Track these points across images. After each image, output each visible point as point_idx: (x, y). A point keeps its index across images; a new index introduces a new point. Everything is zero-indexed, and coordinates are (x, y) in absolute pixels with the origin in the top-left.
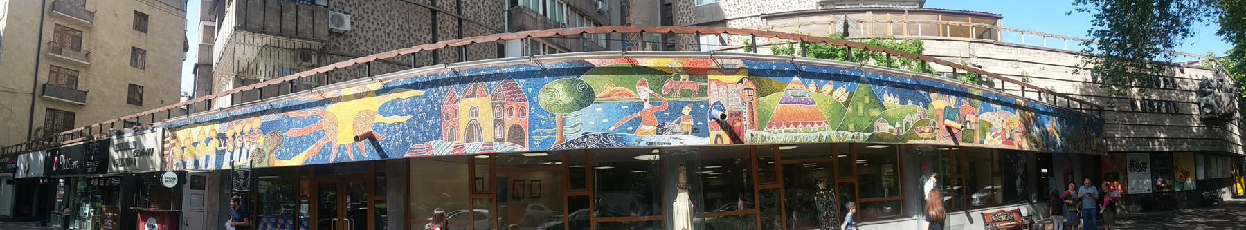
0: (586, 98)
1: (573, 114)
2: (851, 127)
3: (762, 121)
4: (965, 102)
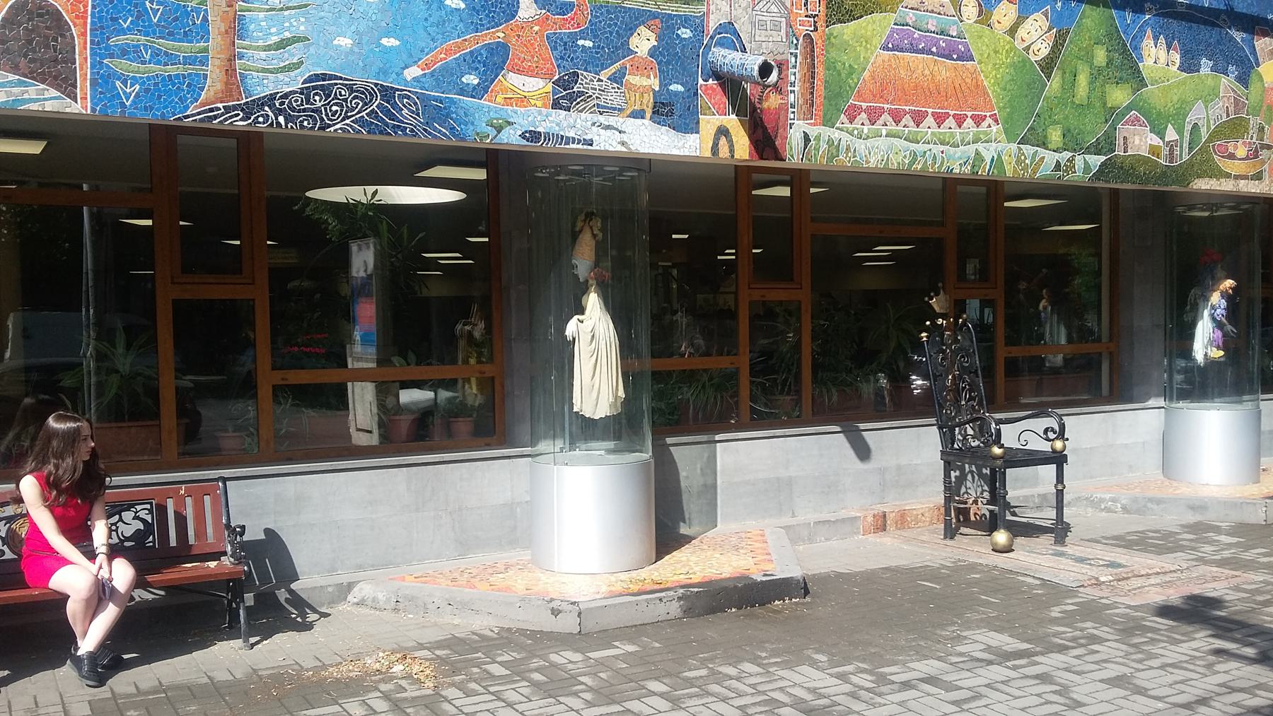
2: (1055, 136)
3: (833, 101)
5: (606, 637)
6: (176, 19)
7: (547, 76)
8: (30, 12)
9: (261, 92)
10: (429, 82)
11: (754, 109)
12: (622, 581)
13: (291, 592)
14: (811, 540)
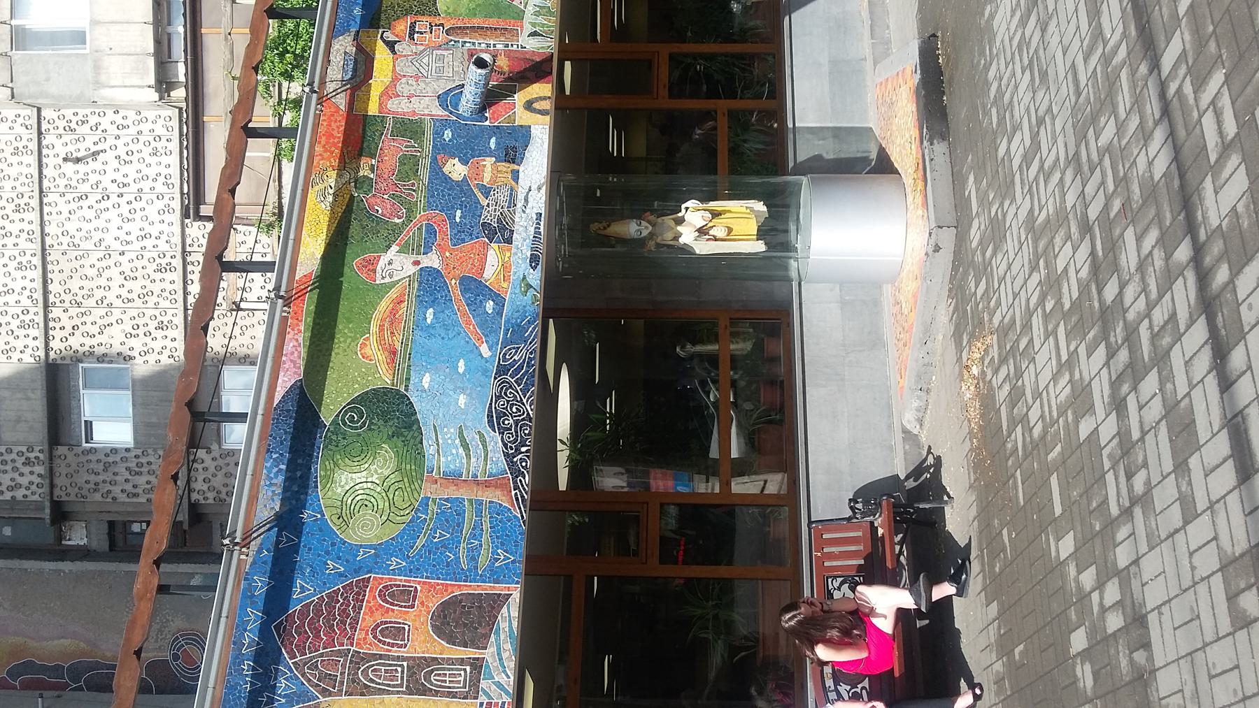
0: (390, 413)
1: (429, 449)
5: (961, 203)
6: (447, 521)
7: (485, 247)
8: (443, 624)
9: (503, 463)
10: (492, 339)
11: (509, 79)
12: (915, 199)
13: (907, 477)
14: (888, 42)
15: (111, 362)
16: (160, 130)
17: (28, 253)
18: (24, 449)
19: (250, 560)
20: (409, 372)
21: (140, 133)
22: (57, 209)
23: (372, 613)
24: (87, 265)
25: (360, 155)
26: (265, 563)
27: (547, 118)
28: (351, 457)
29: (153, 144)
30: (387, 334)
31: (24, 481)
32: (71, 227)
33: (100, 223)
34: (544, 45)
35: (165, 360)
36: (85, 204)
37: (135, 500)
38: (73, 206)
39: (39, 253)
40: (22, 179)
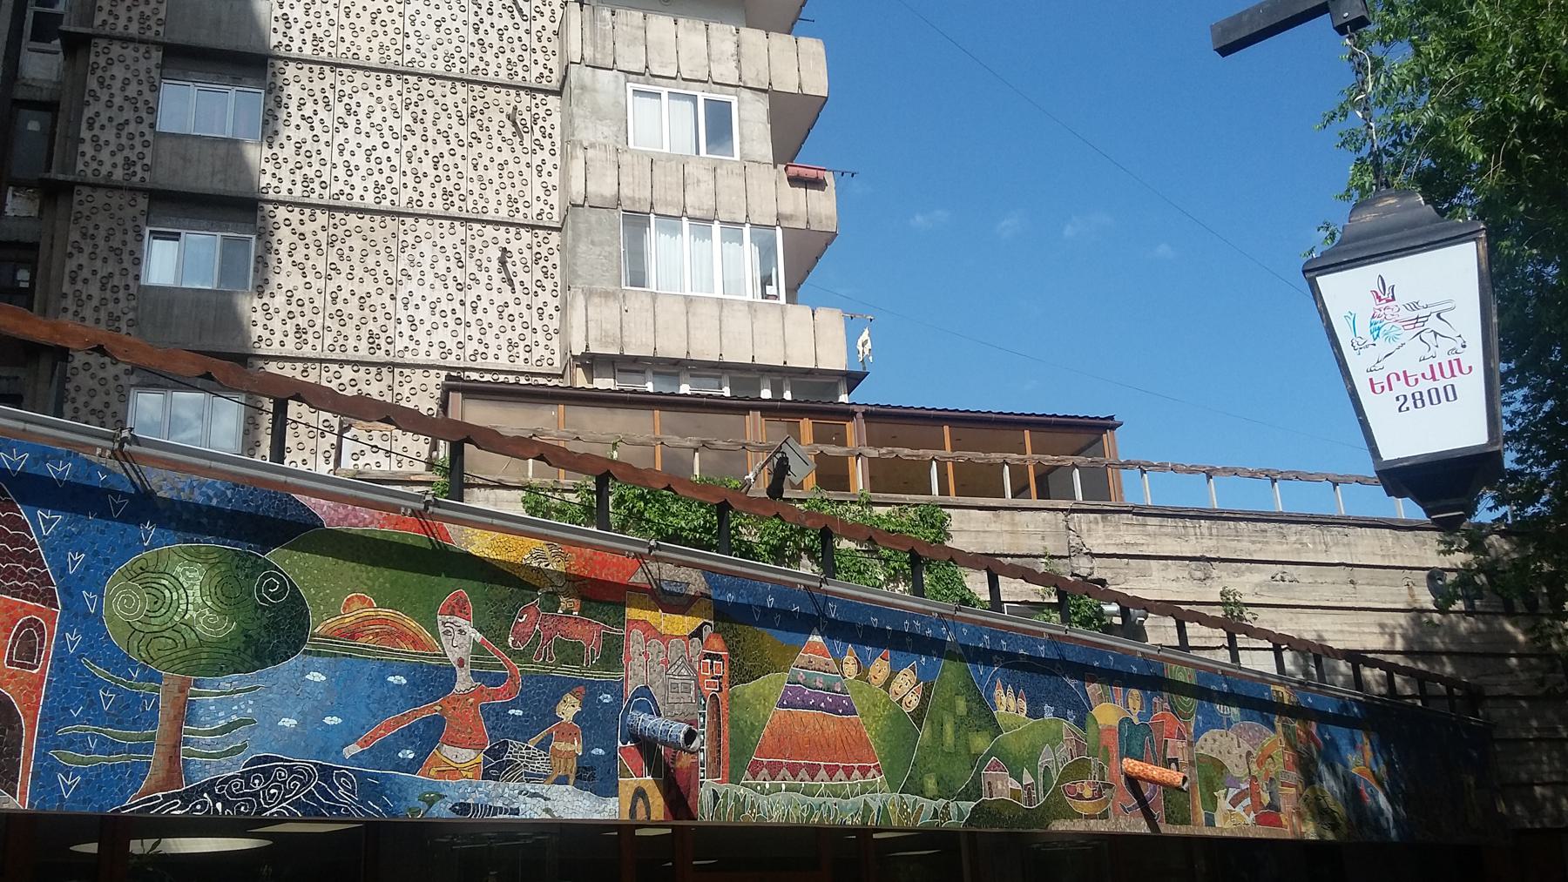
0: (275, 633)
1: (227, 682)
2: (931, 784)
3: (738, 758)
4: (1161, 702)
6: (127, 706)
7: (478, 747)
11: (668, 768)
15: (256, 270)
16: (538, 352)
17: (395, 198)
18: (147, 161)
19: (94, 459)
20: (327, 654)
21: (534, 331)
22: (446, 234)
23: (7, 611)
24: (379, 258)
25: (583, 599)
26: (89, 477)
27: (626, 817)
28: (222, 585)
29: (522, 344)
30: (377, 628)
31: (104, 155)
32: (425, 246)
33: (429, 278)
34: (705, 813)
35: (257, 331)
36: (453, 264)
37: (67, 278)
38: (450, 252)
39: (395, 209)
40: (481, 203)
